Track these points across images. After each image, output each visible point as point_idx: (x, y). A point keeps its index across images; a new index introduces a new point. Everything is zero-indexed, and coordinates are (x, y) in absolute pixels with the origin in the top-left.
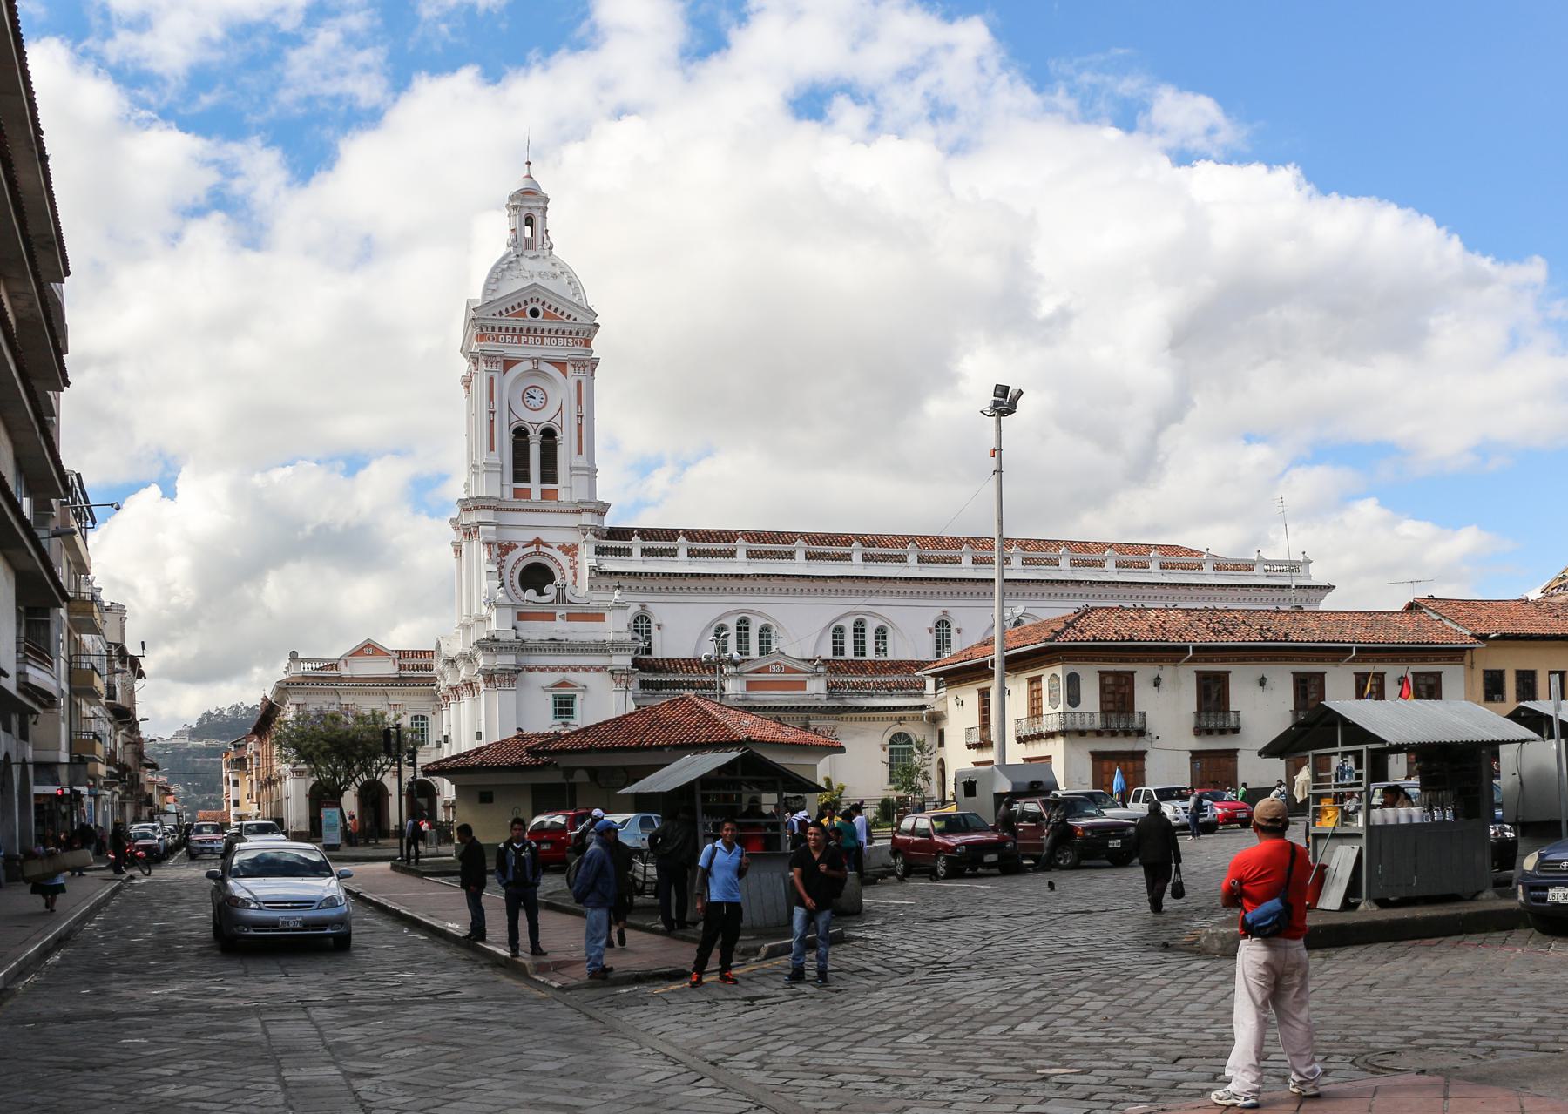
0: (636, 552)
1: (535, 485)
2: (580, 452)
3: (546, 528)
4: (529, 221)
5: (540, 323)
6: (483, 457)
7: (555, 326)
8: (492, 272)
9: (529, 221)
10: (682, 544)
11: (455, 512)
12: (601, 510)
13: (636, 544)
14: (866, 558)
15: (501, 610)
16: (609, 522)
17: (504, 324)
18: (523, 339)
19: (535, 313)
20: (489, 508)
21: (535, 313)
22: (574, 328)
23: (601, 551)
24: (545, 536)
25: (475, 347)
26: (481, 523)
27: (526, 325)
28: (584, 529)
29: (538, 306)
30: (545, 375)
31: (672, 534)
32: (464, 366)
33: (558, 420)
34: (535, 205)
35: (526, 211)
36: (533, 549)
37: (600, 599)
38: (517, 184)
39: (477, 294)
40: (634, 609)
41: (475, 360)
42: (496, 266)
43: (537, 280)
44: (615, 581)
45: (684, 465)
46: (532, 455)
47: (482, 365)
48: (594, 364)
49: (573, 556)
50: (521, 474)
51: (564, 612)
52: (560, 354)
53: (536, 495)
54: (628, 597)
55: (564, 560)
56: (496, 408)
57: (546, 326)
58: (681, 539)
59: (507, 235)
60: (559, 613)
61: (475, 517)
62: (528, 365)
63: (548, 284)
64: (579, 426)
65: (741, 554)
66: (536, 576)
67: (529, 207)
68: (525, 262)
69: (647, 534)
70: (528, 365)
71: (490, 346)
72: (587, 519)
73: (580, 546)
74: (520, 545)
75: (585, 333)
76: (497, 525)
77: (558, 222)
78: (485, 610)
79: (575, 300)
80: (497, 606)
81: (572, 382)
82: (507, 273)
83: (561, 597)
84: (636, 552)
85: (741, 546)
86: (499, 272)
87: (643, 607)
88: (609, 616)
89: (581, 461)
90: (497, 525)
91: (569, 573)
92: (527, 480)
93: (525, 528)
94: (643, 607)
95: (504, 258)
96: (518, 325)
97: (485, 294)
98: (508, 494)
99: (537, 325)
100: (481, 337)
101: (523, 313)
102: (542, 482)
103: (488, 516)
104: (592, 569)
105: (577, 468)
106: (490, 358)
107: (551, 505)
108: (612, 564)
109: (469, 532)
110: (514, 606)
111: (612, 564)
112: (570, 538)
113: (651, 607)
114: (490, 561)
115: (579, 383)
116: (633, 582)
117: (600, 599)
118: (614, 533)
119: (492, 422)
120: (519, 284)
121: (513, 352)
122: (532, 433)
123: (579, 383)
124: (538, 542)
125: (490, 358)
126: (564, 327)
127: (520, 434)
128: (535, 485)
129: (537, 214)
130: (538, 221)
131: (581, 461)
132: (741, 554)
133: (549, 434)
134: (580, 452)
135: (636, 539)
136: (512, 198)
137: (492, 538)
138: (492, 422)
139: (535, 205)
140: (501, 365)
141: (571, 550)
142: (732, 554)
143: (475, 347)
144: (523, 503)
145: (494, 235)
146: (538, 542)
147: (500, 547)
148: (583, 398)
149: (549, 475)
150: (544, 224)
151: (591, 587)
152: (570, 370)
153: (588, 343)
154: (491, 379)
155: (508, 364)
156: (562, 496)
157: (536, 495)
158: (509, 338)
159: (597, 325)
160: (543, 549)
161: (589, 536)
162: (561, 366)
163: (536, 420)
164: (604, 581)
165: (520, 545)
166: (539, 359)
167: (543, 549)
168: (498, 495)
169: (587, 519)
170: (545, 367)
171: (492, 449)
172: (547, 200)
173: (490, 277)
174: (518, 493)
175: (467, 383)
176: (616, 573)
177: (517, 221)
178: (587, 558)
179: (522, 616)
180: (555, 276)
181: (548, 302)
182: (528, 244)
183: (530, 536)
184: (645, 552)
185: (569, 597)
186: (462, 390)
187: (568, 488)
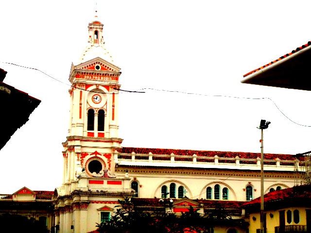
0: (195, 160)
1: (96, 131)
24: (99, 151)
28: (113, 148)
29: (99, 65)
35: (94, 30)
36: (94, 155)
37: (119, 176)
40: (132, 179)
50: (91, 127)
52: (106, 83)
53: (96, 135)
57: (102, 73)
62: (94, 87)
69: (137, 150)
74: (89, 154)
83: (105, 176)
84: (195, 160)
87: (135, 179)
91: (107, 165)
92: (93, 130)
93: (90, 148)
94: (250, 183)
98: (86, 135)
101: (93, 68)
102: (99, 130)
110: (88, 178)
112: (108, 151)
113: (138, 179)
117: (119, 176)
118: (125, 150)
121: (89, 82)
122: (95, 112)
124: (96, 153)
128: (96, 131)
133: (102, 114)
139: (98, 27)
146: (96, 153)
149: (101, 127)
152: (110, 89)
153: (117, 79)
156: (107, 136)
157: (96, 135)
158: (88, 77)
162: (107, 87)
163: (96, 107)
165: (89, 154)
166: (99, 85)
167: (98, 156)
170: (101, 88)
183: (93, 150)
187: (108, 133)
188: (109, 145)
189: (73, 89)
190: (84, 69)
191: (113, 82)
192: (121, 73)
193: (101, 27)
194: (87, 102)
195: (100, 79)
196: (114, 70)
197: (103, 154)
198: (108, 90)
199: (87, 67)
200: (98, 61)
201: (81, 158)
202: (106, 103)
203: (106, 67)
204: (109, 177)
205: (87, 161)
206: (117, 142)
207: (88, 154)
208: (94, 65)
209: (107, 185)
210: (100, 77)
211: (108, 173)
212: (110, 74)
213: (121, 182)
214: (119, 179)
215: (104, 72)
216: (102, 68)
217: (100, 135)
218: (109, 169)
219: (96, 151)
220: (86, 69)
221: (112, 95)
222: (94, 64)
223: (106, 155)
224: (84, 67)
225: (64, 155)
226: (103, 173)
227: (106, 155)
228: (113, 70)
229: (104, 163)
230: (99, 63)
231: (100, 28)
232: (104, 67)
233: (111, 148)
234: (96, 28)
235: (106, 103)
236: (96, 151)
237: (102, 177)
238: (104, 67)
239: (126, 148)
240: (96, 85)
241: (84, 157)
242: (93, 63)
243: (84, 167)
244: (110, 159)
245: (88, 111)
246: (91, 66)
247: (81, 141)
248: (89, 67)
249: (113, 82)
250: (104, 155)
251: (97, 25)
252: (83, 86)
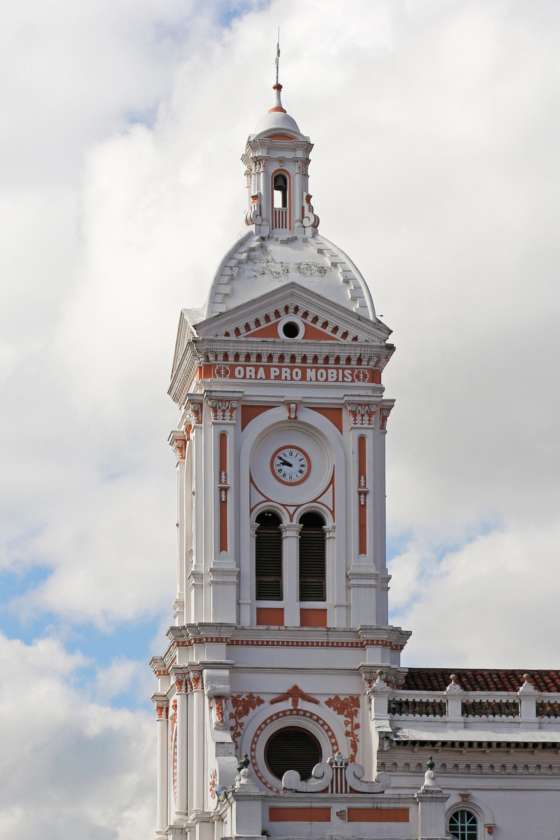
0: (454, 709)
1: (291, 603)
2: (362, 550)
3: (307, 673)
4: (280, 182)
5: (299, 345)
6: (206, 562)
7: (324, 351)
8: (224, 265)
9: (280, 182)
10: (453, 695)
11: (162, 644)
12: (397, 640)
13: (453, 695)
14: (469, 709)
15: (246, 804)
16: (411, 658)
17: (243, 349)
18: (274, 372)
19: (291, 330)
20: (219, 640)
21: (291, 330)
22: (355, 353)
23: (397, 708)
24: (307, 685)
25: (195, 386)
26: (206, 665)
27: (278, 350)
28: (369, 673)
29: (297, 319)
30: (309, 430)
31: (509, 679)
32: (175, 416)
33: (327, 499)
34: (289, 155)
35: (274, 167)
36: (287, 705)
37: (400, 785)
38: (260, 122)
39: (199, 305)
40: (454, 799)
41: (196, 406)
42: (230, 256)
43: (294, 277)
44: (425, 756)
45: (444, 551)
46: (286, 554)
47: (208, 415)
48: (386, 408)
49: (352, 715)
50: (268, 584)
51: (344, 807)
52: (331, 396)
53: (292, 619)
54: (444, 782)
55: (336, 721)
56: (230, 482)
57: (310, 351)
58: (526, 688)
59: (247, 207)
60: (336, 808)
61: (196, 656)
62: (279, 414)
63: (312, 283)
64: (362, 508)
65: (528, 710)
66: (292, 749)
67: (281, 157)
68: (276, 250)
69: (471, 679)
70: (279, 414)
71: (221, 385)
72: (374, 657)
73: (363, 700)
74: (267, 699)
75: (371, 353)
76: (231, 667)
77: (323, 180)
78: (211, 804)
79: (355, 308)
80: (238, 797)
81: (351, 440)
82: (247, 268)
83: (338, 783)
84: (454, 709)
85: (527, 695)
86: (238, 263)
87: (465, 797)
88: (417, 812)
89: (365, 564)
90: (231, 667)
91: (344, 743)
92: (278, 596)
93: (275, 670)
94: (465, 797)
95: (241, 243)
96: (265, 349)
97: (213, 301)
98: (248, 618)
99: (296, 350)
100: (207, 370)
101: (272, 331)
102: (303, 597)
103: (218, 653)
104: (384, 737)
105: (360, 576)
106: (220, 404)
107: (315, 634)
108: (415, 730)
109: (187, 680)
110: (264, 798)
111: (415, 730)
112: (345, 687)
113: (478, 797)
114: (221, 726)
115: (362, 440)
116: (449, 758)
117: (400, 785)
118: (420, 678)
119: (223, 505)
120: (269, 285)
121: (256, 393)
122: (286, 521)
123: (362, 440)
124: (295, 693)
125: (220, 404)
126: (337, 351)
127: (268, 522)
128: (291, 603)
129: (292, 170)
130: (295, 182)
131: (365, 564)
132: (528, 710)
133: (312, 522)
134: (362, 550)
135: (453, 688)
136: (252, 144)
137: (224, 688)
138: (223, 505)
139: (289, 155)
140: (237, 414)
141: (347, 706)
142: (512, 709)
143: (195, 386)
144: (271, 633)
145: (226, 203)
146: (295, 693)
147: (235, 702)
148: (368, 465)
149: (313, 584)
150: (305, 186)
151: (381, 766)
152: (347, 419)
153: (376, 376)
154: (223, 437)
155: (250, 412)
156: (334, 620)
157: (292, 619)
158: (251, 371)
159: (391, 348)
160: (303, 705)
161: (378, 683)
162: (333, 413)
163: (291, 501)
164: (403, 756)
165: (267, 699)
166: (298, 404)
167: (303, 705)
168: (231, 619)
169: (374, 657)
171: (223, 546)
172: (309, 147)
173: (221, 274)
174: (264, 617)
175: (181, 443)
176: (423, 743)
177: (261, 184)
178: (375, 722)
179: (276, 814)
180: (322, 270)
181: (313, 312)
182: (279, 219)
183: (283, 684)
184: (469, 709)
185: (352, 782)
186: (172, 455)
187: (340, 604)
188: (349, 658)
189: (189, 429)
190: (233, 337)
191: (361, 390)
192: (391, 348)
193: (300, 154)
194: (251, 480)
195: (304, 378)
196: (362, 337)
197: (323, 700)
198: (339, 425)
199: (247, 327)
200: (293, 302)
201: (232, 716)
202: (332, 482)
203: (325, 325)
204: (352, 791)
205: (260, 729)
206: (384, 644)
207: (260, 702)
208: (274, 320)
209: (300, 783)
210: (304, 370)
211: (349, 773)
212: (344, 356)
213: (406, 811)
214: (399, 799)
215: (322, 349)
216: (310, 333)
217: (307, 617)
218: (353, 759)
219: (296, 687)
220: (241, 338)
221: (180, 830)
222: (277, 314)
223: (335, 703)
224: (231, 329)
225: (160, 709)
226: (329, 773)
227: (335, 703)
228: (355, 339)
229: (333, 736)
230: (296, 309)
231: (295, 160)
232: (318, 326)
233: (356, 672)
234: (281, 160)
235: (332, 482)
236: (296, 687)
237: (325, 791)
238: (318, 326)
239: (420, 671)
240: (288, 404)
241: (246, 712)
242: (270, 311)
243: (246, 749)
244: (356, 720)
245: (258, 520)
246: (264, 325)
247: (231, 643)
248: (254, 329)
249: (361, 390)
250: (329, 703)
251: (281, 149)
252: (232, 410)
